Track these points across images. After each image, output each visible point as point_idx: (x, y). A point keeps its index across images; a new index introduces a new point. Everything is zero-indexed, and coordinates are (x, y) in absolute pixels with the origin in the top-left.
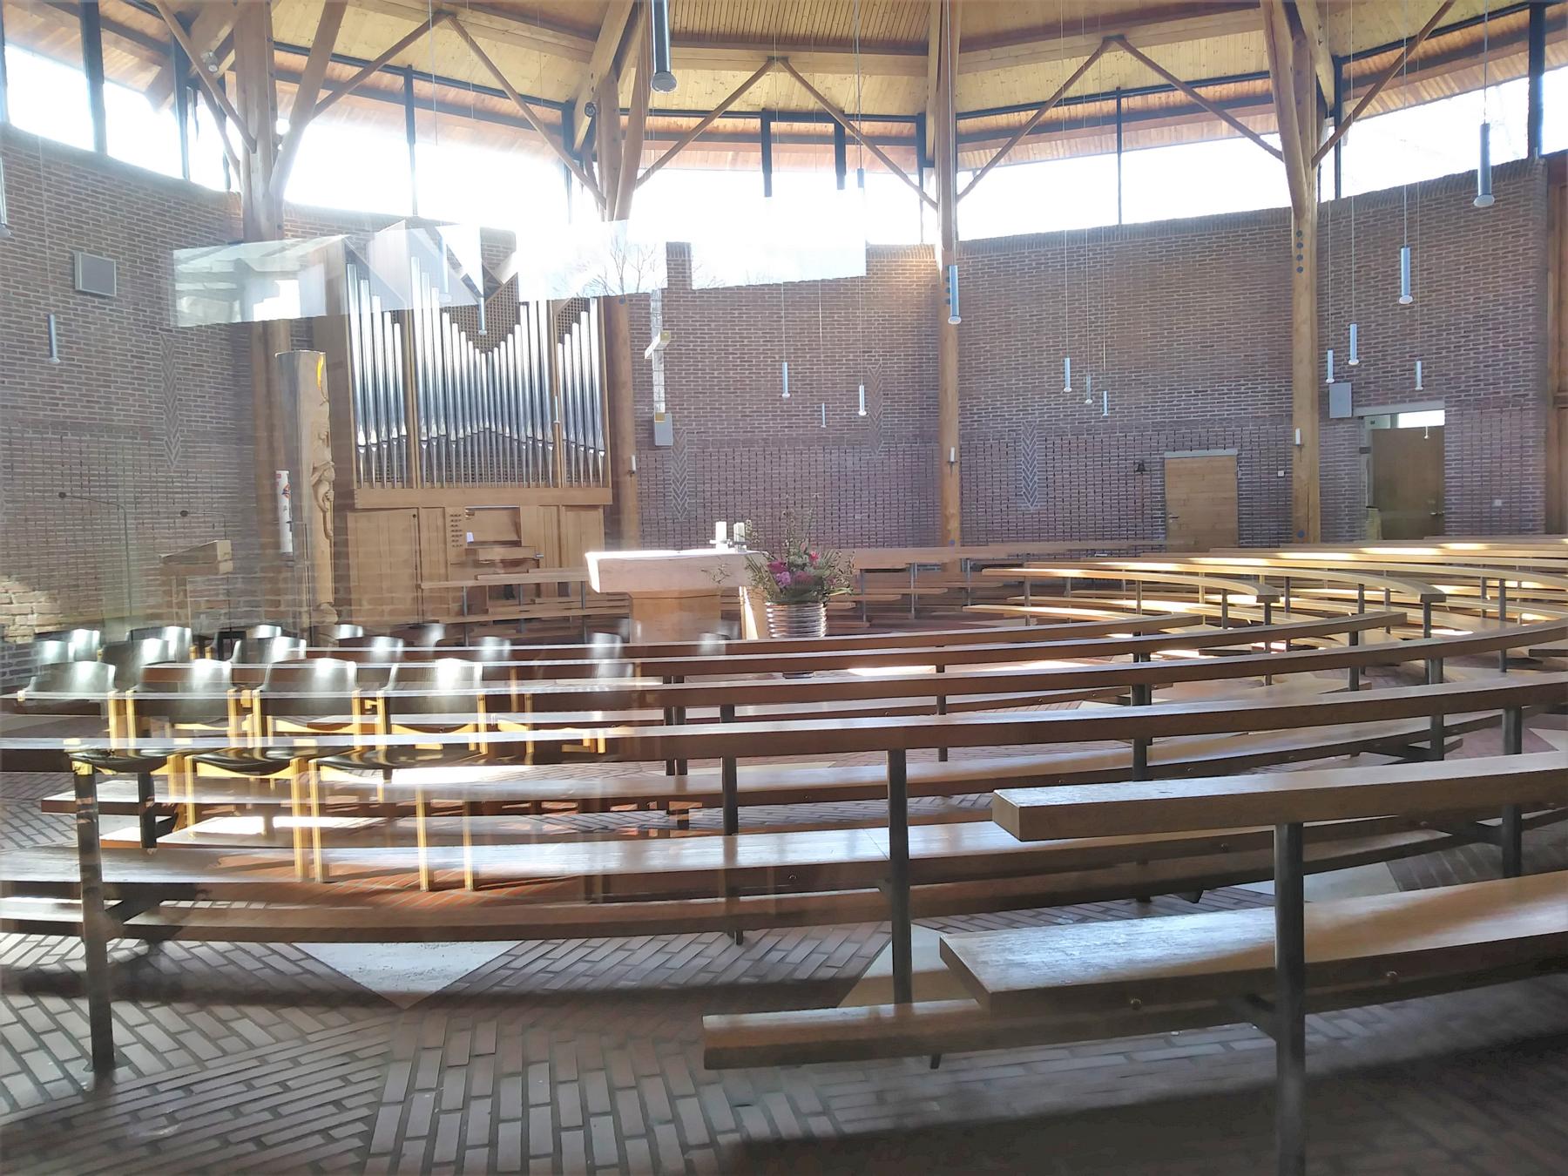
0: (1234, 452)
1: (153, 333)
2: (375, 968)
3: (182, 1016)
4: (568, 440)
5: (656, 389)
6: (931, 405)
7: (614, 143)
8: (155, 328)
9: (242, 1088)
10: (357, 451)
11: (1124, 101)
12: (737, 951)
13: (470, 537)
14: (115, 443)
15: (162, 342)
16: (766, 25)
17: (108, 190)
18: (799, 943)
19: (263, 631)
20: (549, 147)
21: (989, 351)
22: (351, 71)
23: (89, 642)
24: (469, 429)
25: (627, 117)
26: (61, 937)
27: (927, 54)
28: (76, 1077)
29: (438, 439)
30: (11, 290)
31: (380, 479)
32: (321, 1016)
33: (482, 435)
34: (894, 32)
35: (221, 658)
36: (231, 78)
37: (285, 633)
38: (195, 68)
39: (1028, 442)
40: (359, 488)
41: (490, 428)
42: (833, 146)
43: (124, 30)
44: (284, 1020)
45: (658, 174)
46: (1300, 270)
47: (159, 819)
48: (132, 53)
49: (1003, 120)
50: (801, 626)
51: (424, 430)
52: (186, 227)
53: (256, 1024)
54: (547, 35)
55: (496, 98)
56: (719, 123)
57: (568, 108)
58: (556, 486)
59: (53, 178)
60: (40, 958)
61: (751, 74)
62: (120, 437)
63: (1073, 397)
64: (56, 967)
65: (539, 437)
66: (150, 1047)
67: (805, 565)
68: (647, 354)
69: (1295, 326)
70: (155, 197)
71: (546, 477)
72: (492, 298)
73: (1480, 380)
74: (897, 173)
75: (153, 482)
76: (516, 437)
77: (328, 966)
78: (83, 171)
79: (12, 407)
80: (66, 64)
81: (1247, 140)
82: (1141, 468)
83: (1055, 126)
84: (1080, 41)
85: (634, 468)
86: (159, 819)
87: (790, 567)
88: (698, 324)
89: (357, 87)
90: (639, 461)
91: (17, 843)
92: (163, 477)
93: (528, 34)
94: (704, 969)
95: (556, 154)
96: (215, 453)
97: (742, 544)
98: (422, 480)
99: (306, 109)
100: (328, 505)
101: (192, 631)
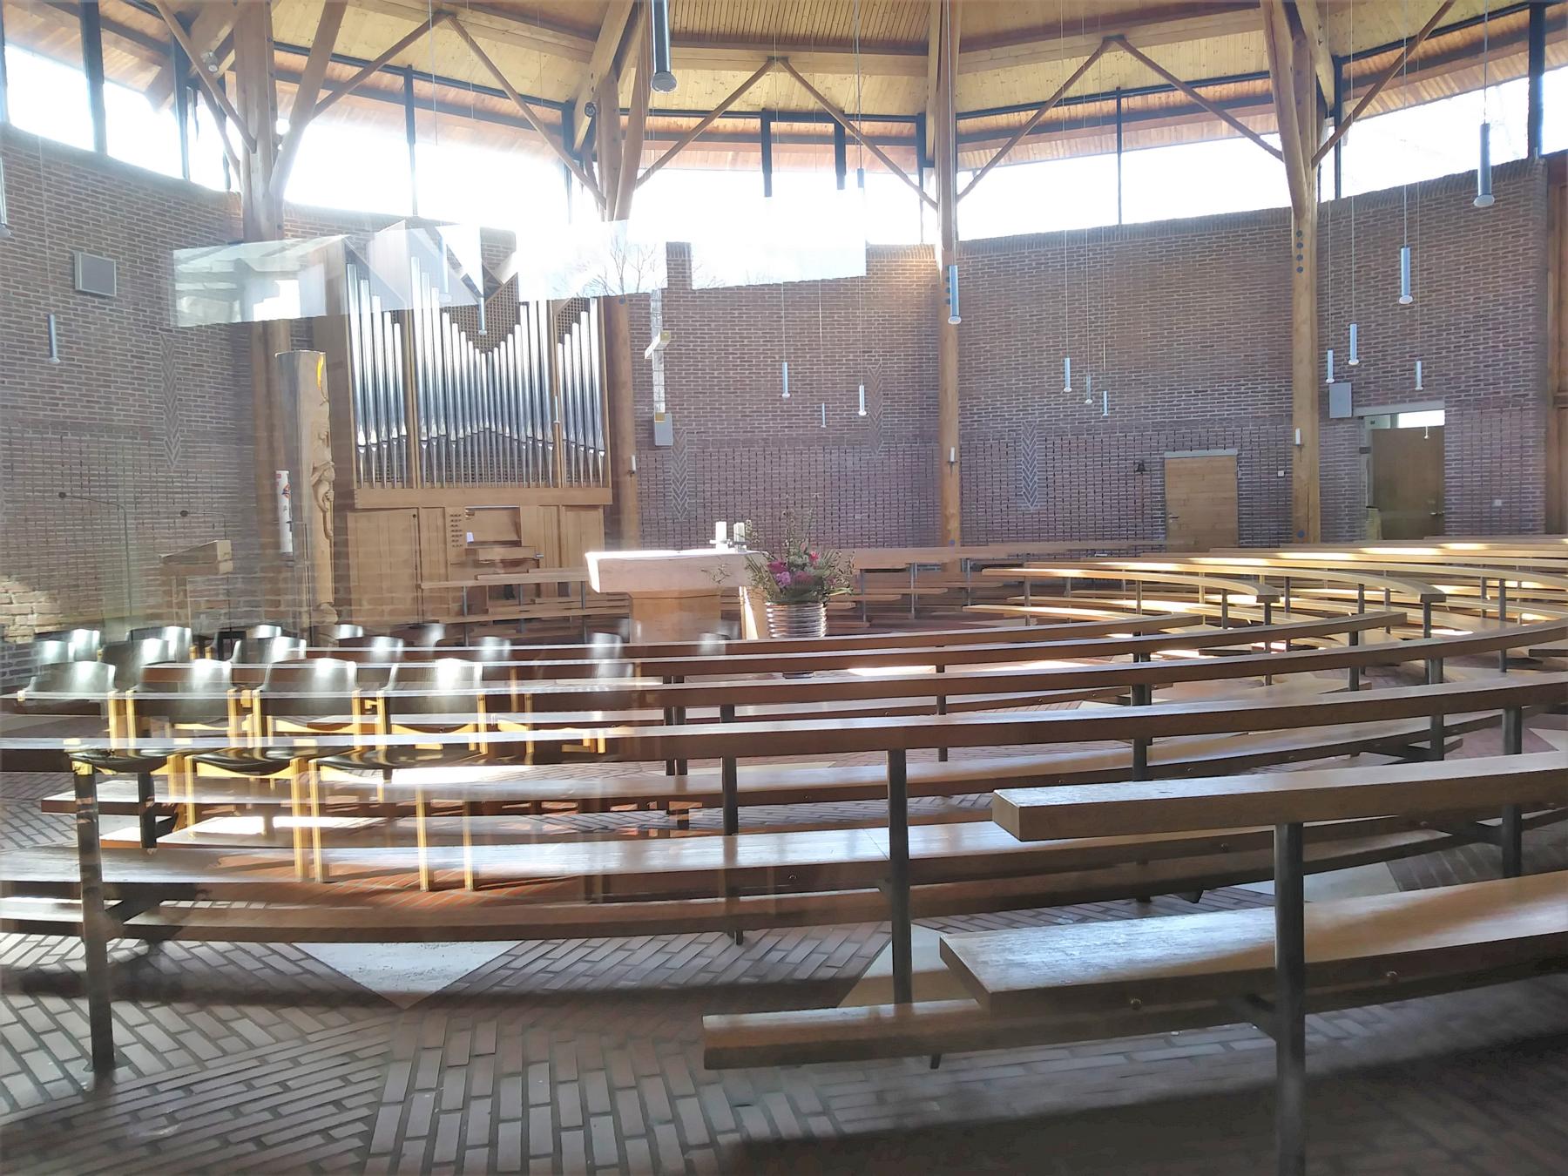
0: (1234, 452)
1: (153, 333)
2: (375, 968)
3: (182, 1016)
4: (568, 440)
5: (656, 389)
6: (931, 405)
7: (614, 143)
8: (155, 328)
9: (242, 1088)
10: (357, 451)
11: (1124, 101)
12: (737, 951)
13: (470, 537)
14: (115, 443)
15: (162, 342)
16: (766, 25)
17: (108, 190)
18: (799, 943)
19: (263, 631)
20: (549, 147)
21: (989, 351)
22: (351, 71)
23: (89, 642)
24: (469, 429)
25: (627, 117)
26: (61, 937)
27: (927, 54)
28: (76, 1077)
29: (438, 439)
30: (11, 290)
31: (380, 479)
32: (321, 1016)
33: (482, 435)
34: (894, 32)
35: (221, 658)
36: (231, 78)
37: (285, 633)
38: (195, 68)
39: (1028, 442)
40: (359, 488)
41: (490, 428)
42: (833, 146)
43: (124, 30)
44: (284, 1020)
45: (658, 174)
46: (1300, 270)
47: (159, 819)
48: (132, 53)
49: (1003, 120)
50: (801, 626)
51: (424, 430)
52: (186, 227)
53: (256, 1024)
54: (547, 35)
55: (496, 98)
56: (719, 123)
57: (568, 108)
58: (556, 486)
59: (53, 178)
60: (40, 958)
61: (751, 74)
62: (120, 437)
63: (1073, 397)
64: (56, 967)
65: (539, 437)
66: (150, 1047)
67: (805, 565)
68: (647, 354)
69: (1295, 326)
70: (155, 197)
71: (546, 477)
72: (492, 298)
73: (1480, 380)
74: (897, 173)
75: (153, 482)
76: (516, 437)
77: (328, 966)
78: (83, 171)
79: (12, 407)
80: (66, 64)
81: (1247, 140)
82: (1141, 468)
83: (1055, 126)
84: (1080, 41)
85: (634, 468)
86: (159, 819)
87: (790, 567)
88: (698, 324)
89: (357, 87)
90: (639, 461)
91: (17, 843)
92: (163, 477)
93: (528, 34)
94: (704, 969)
95: (556, 154)
96: (215, 453)
97: (742, 544)
98: (422, 480)
99: (306, 109)
100: (328, 505)
101: (192, 631)
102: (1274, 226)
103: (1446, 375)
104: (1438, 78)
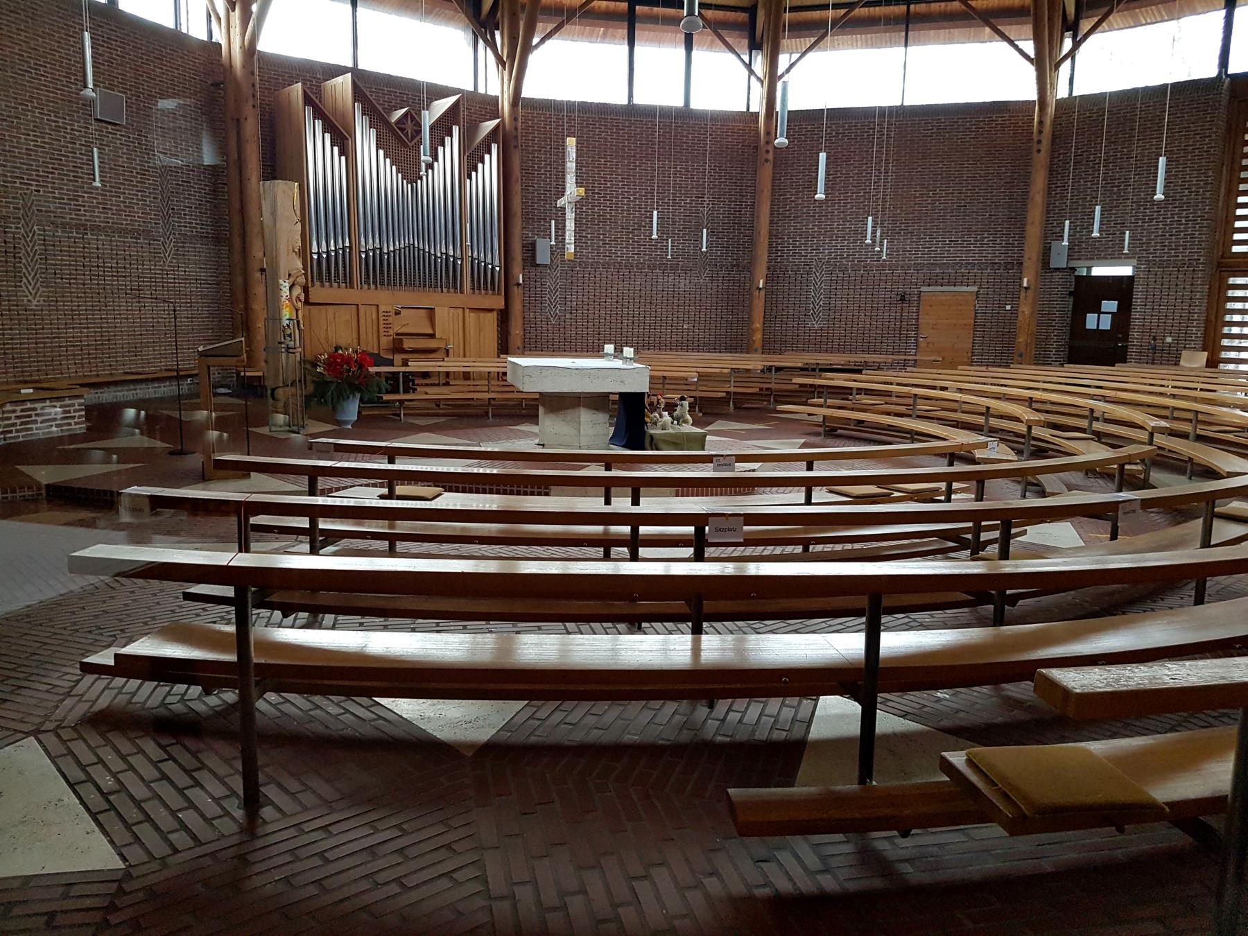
0: (975, 289)
4: (472, 257)
10: (311, 257)
11: (912, 7)
21: (793, 201)
29: (374, 250)
33: (407, 249)
41: (414, 244)
45: (549, 43)
46: (1039, 151)
51: (363, 243)
65: (451, 253)
69: (1031, 194)
71: (455, 285)
73: (1165, 246)
74: (732, 53)
75: (152, 273)
81: (1005, 45)
82: (903, 299)
98: (361, 283)
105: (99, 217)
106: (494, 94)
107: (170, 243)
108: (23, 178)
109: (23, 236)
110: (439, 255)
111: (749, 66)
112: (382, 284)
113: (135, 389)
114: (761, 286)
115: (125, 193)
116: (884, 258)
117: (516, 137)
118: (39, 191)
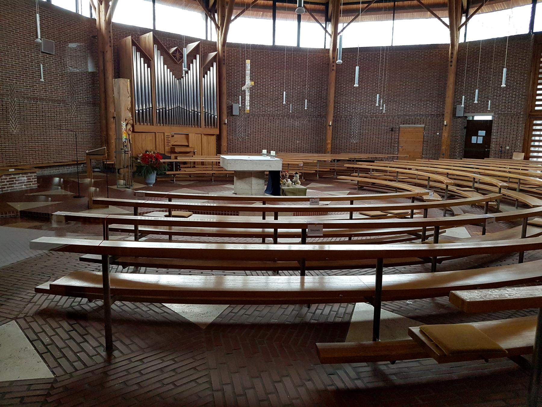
0: (423, 126)
4: (205, 112)
10: (135, 112)
11: (396, 3)
21: (344, 88)
29: (162, 109)
33: (177, 108)
41: (180, 106)
45: (238, 19)
46: (451, 66)
51: (158, 106)
65: (196, 110)
69: (448, 84)
71: (197, 124)
73: (506, 107)
74: (318, 23)
75: (66, 119)
81: (436, 19)
82: (392, 130)
98: (157, 123)
102: (443, 50)
103: (495, 104)
104: (501, 3)
105: (43, 94)
106: (214, 41)
107: (74, 106)
108: (10, 78)
109: (10, 102)
110: (191, 111)
111: (325, 29)
112: (166, 123)
113: (59, 169)
114: (330, 124)
115: (54, 84)
116: (384, 112)
117: (224, 60)
118: (17, 83)
